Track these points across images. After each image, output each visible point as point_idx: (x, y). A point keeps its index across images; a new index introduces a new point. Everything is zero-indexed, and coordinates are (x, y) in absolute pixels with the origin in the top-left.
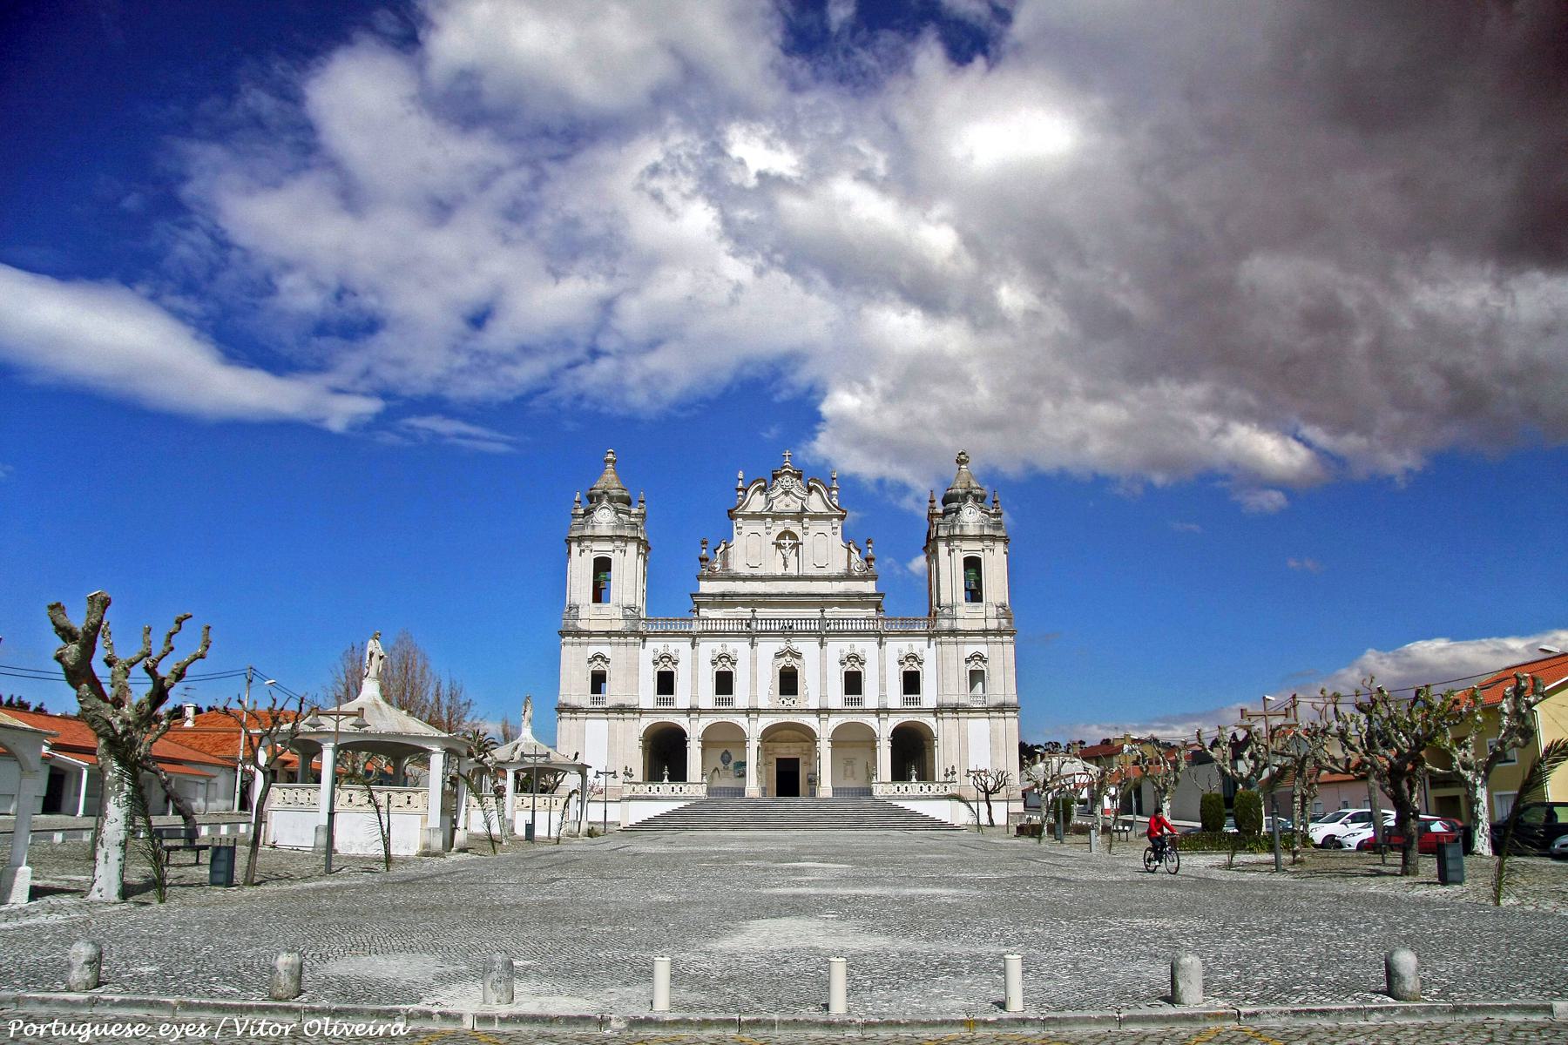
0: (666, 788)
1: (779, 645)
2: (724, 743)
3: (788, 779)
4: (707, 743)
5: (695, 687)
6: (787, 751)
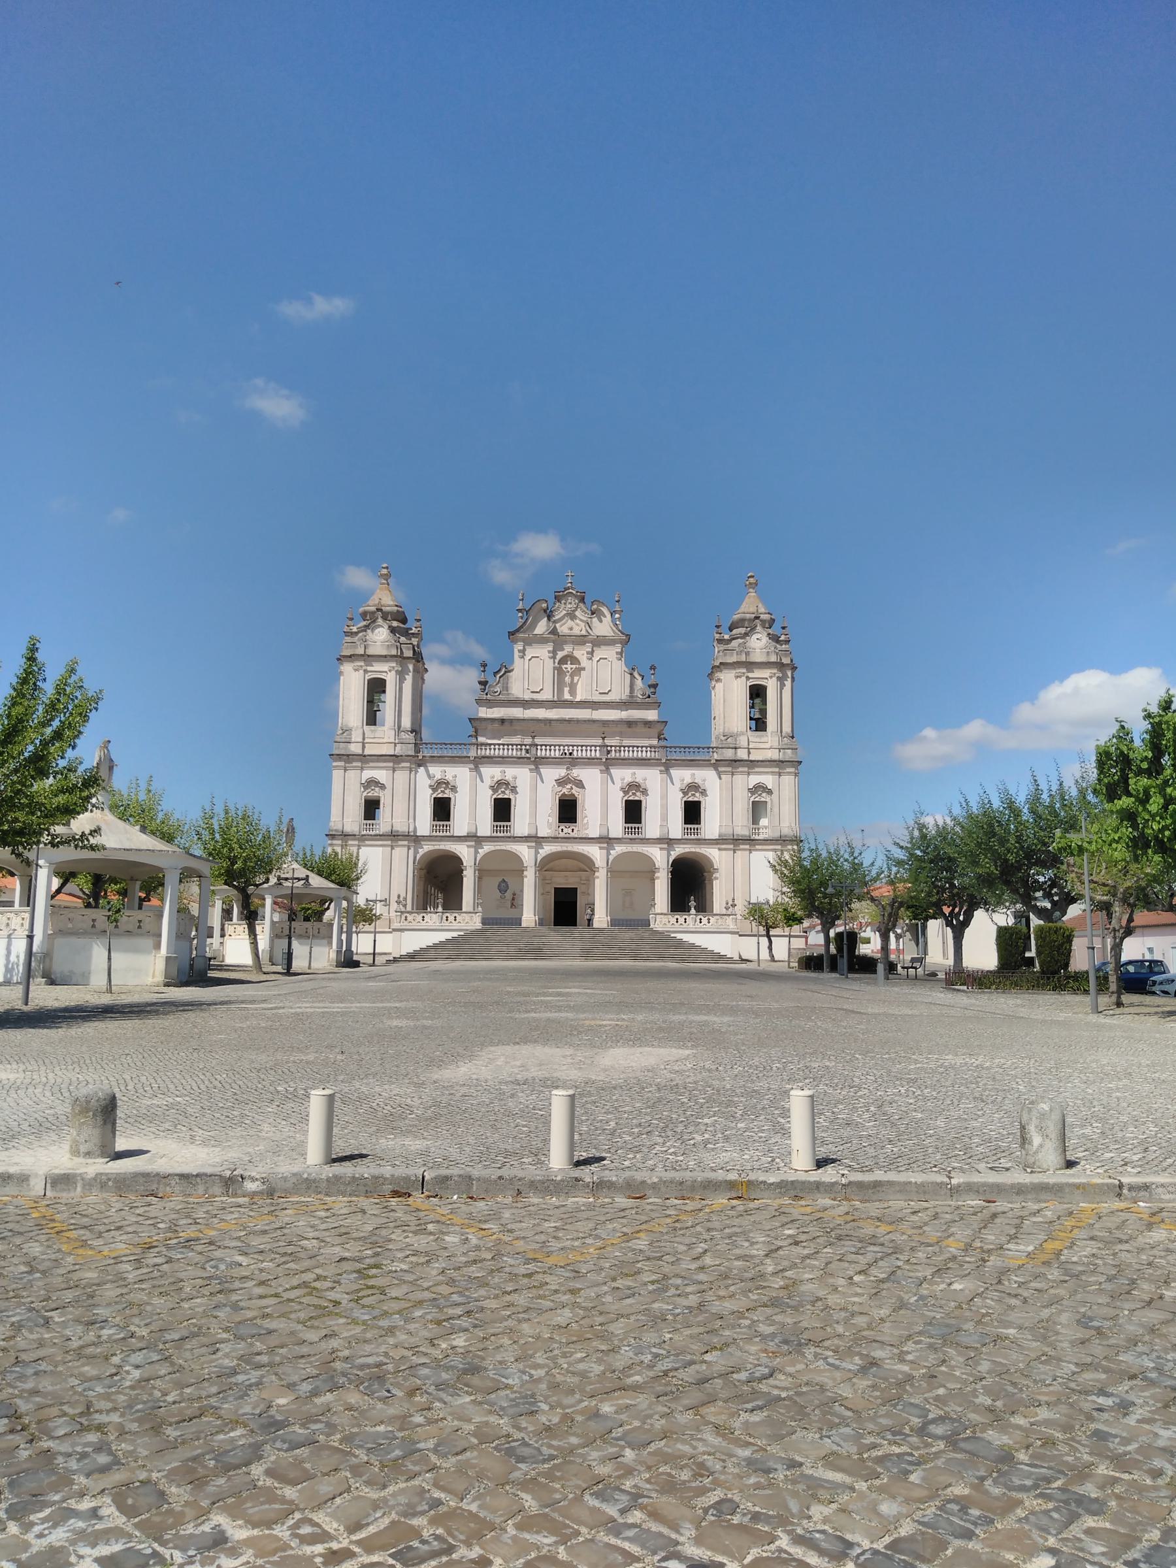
0: (432, 919)
1: (561, 772)
2: (502, 877)
3: (565, 909)
4: (482, 873)
5: (472, 812)
6: (565, 881)
